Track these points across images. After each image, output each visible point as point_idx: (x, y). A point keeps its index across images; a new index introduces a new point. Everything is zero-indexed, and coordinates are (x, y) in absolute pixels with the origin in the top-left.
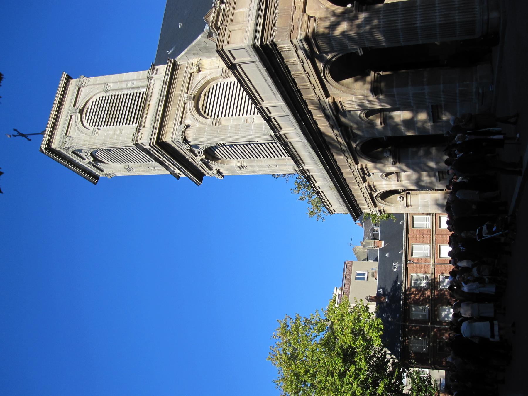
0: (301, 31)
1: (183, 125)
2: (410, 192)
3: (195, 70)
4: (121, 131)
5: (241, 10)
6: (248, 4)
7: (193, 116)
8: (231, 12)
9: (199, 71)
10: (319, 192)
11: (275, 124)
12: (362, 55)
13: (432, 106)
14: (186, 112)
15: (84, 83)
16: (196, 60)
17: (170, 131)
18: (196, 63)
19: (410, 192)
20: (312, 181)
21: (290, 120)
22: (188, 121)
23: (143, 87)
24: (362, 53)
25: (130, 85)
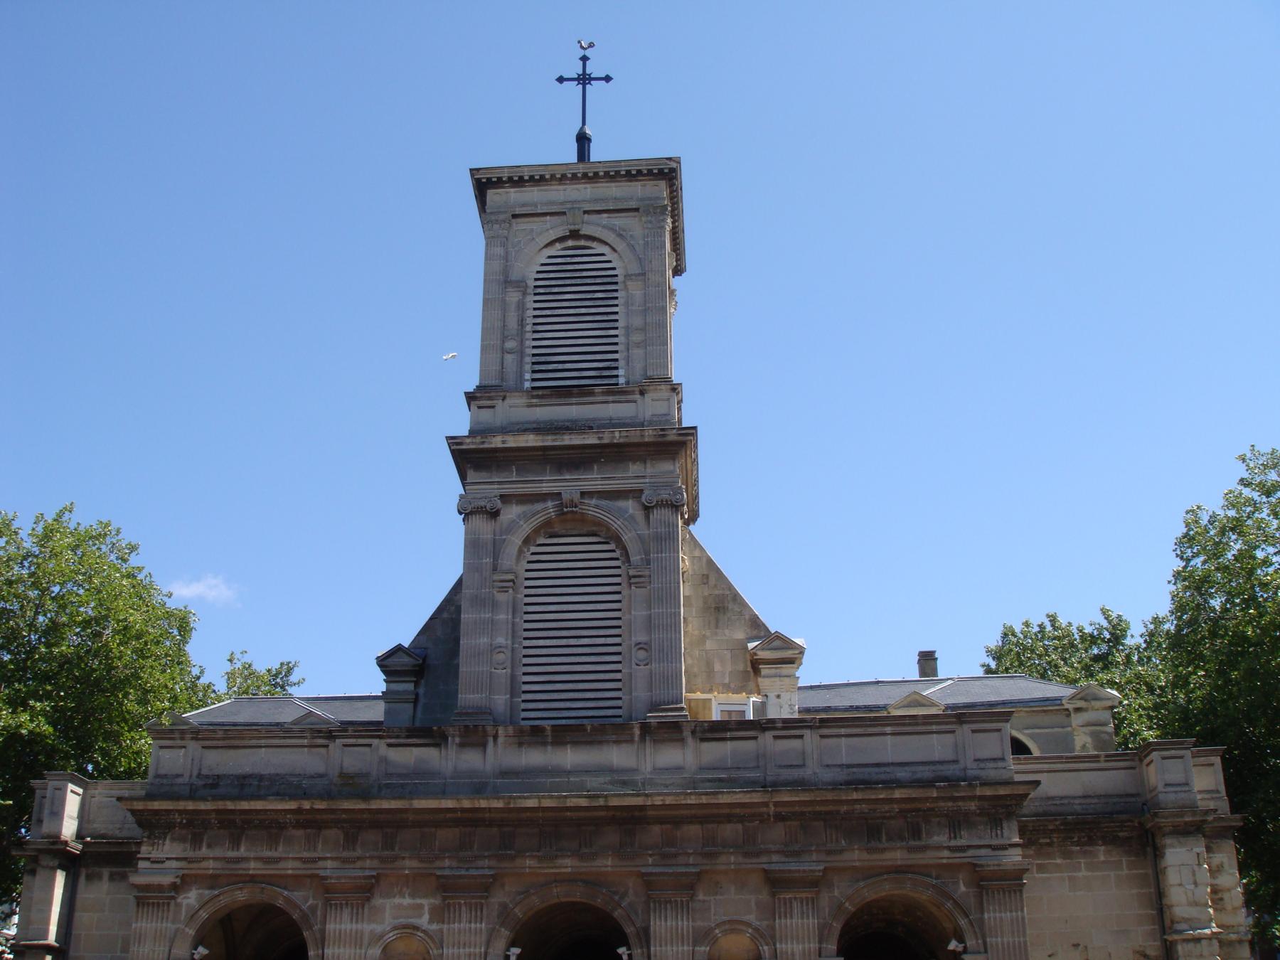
11: (728, 735)
20: (408, 737)
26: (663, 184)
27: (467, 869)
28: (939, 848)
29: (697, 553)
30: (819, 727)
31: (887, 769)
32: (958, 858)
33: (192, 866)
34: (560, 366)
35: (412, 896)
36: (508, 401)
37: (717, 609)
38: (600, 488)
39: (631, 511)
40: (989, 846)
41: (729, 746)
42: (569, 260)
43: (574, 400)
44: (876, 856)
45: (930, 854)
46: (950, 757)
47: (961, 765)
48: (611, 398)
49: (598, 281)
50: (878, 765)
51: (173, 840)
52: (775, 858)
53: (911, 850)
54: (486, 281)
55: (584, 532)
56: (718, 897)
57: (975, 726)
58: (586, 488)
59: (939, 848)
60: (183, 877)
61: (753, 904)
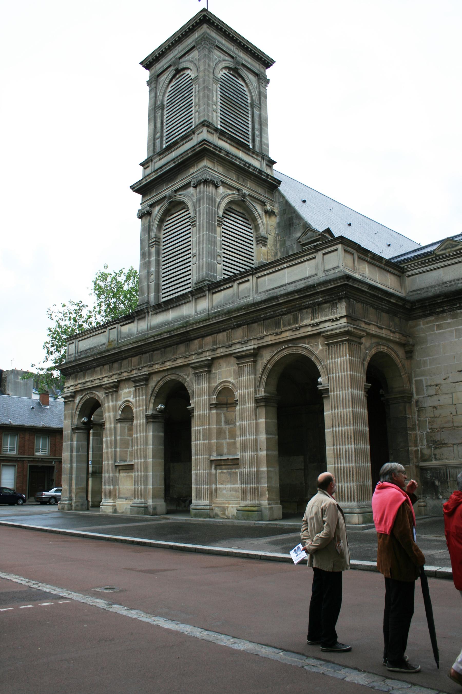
0: (354, 328)
1: (220, 183)
2: (455, 428)
3: (268, 207)
4: (215, 111)
5: (367, 269)
6: (371, 277)
7: (227, 196)
8: (366, 258)
9: (266, 212)
10: (106, 328)
11: (222, 288)
12: (318, 388)
13: (133, 465)
14: (229, 189)
15: (263, 82)
16: (276, 211)
17: (214, 166)
18: (274, 211)
19: (455, 428)
20: (125, 321)
21: (229, 304)
22: (221, 189)
23: (254, 146)
24: (319, 389)
25: (257, 133)
26: (205, 26)
27: (140, 373)
28: (306, 326)
29: (281, 200)
30: (256, 273)
31: (284, 288)
32: (316, 330)
33: (76, 387)
34: (174, 136)
35: (129, 388)
36: (154, 161)
37: (290, 225)
38: (180, 186)
39: (192, 192)
40: (329, 320)
41: (223, 293)
42: (177, 84)
43: (173, 149)
44: (278, 337)
45: (302, 330)
46: (313, 273)
47: (318, 277)
48: (184, 142)
49: (187, 88)
50: (281, 286)
51: (72, 378)
52: (238, 346)
53: (294, 330)
54: (149, 111)
55: (180, 209)
56: (220, 370)
57: (324, 251)
58: (174, 189)
59: (306, 326)
60: (75, 392)
61: (232, 371)
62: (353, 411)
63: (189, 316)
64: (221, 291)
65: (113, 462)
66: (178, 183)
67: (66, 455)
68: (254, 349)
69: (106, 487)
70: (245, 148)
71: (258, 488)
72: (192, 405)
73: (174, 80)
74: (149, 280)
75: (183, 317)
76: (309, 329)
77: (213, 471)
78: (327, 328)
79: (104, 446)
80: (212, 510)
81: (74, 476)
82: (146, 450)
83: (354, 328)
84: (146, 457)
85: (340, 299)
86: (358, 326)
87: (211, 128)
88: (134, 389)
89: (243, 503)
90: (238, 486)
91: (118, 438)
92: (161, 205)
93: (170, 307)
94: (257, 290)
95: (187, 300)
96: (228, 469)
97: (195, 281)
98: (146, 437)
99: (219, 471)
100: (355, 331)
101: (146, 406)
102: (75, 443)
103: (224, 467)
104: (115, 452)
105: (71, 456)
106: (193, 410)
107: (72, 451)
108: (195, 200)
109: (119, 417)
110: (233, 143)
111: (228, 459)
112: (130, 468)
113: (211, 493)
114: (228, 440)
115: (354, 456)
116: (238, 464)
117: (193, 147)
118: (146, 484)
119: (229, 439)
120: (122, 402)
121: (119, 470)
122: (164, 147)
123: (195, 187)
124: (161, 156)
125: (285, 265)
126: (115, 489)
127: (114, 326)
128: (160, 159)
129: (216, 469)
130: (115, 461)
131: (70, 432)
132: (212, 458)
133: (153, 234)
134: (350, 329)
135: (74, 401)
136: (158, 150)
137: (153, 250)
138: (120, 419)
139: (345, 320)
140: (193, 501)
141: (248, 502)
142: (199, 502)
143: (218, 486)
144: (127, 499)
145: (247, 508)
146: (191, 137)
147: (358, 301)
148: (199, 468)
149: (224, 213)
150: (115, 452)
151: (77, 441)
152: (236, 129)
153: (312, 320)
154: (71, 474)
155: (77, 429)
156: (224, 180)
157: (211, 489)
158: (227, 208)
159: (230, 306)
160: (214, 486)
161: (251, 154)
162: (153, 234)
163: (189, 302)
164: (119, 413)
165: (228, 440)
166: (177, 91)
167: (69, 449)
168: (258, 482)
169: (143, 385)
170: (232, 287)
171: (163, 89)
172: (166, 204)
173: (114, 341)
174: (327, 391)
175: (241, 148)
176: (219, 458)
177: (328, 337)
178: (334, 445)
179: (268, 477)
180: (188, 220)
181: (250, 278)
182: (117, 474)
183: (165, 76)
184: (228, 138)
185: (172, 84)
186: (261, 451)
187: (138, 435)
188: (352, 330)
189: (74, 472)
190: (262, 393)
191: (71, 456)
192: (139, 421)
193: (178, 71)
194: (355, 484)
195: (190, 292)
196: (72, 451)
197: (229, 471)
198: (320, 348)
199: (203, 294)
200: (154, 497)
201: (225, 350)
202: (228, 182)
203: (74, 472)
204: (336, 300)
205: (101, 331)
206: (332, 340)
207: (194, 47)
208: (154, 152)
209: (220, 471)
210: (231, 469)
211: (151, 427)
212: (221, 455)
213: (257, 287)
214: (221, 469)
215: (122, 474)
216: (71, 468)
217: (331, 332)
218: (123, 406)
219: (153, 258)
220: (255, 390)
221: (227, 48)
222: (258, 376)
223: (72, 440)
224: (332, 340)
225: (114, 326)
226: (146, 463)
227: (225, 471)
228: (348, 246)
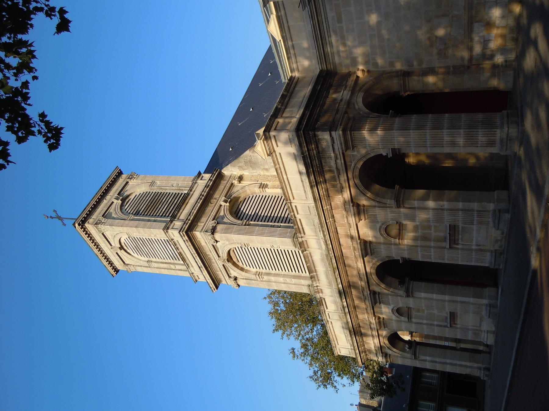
11: (300, 227)
36: (193, 272)
62: (413, 130)
63: (322, 254)
64: (303, 228)
65: (447, 329)
66: (212, 254)
67: (438, 367)
68: (353, 206)
69: (470, 336)
70: (187, 197)
71: (478, 211)
72: (399, 258)
73: (128, 251)
74: (289, 284)
75: (322, 260)
76: (339, 161)
77: (460, 246)
78: (340, 147)
79: (432, 334)
80: (496, 250)
81: (458, 362)
82: (437, 300)
83: (340, 125)
84: (444, 301)
85: (315, 136)
86: (339, 122)
87: (170, 225)
88: (382, 304)
89: (491, 224)
90: (475, 227)
91: (425, 322)
92: (229, 268)
93: (313, 269)
94: (304, 200)
95: (309, 255)
96: (458, 234)
97: (294, 248)
98: (425, 298)
99: (460, 242)
100: (343, 124)
101: (398, 296)
102: (428, 358)
103: (456, 237)
104: (437, 325)
105: (440, 363)
106: (403, 258)
107: (436, 362)
108: (227, 243)
109: (407, 319)
110: (183, 208)
111: (449, 233)
112: (453, 316)
113: (481, 250)
114: (432, 231)
115: (454, 131)
116: (455, 226)
117: (184, 241)
118: (469, 303)
119: (431, 230)
120: (393, 315)
121: (455, 324)
122: (182, 262)
123: (217, 242)
124: (190, 265)
125: (285, 177)
126: (472, 330)
127: (327, 315)
128: (193, 267)
129: (458, 244)
130: (446, 326)
131: (417, 361)
132: (448, 246)
133: (253, 277)
134: (341, 129)
135: (390, 355)
136: (184, 267)
137: (266, 278)
138: (408, 318)
139: (333, 133)
140: (487, 265)
141: (490, 220)
142: (486, 261)
143: (474, 243)
144: (481, 320)
145: (497, 221)
146: (177, 242)
147: (317, 120)
148: (457, 257)
149: (239, 219)
150: (437, 325)
151: (426, 356)
152: (171, 203)
153: (331, 159)
154: (456, 365)
155: (415, 354)
156: (213, 217)
157: (476, 250)
158: (235, 216)
159: (317, 221)
160: (474, 247)
161: (192, 193)
162: (253, 277)
163: (310, 253)
164: (403, 318)
165: (432, 231)
166: (138, 249)
167: (434, 364)
168: (473, 210)
169: (379, 297)
170: (300, 219)
171: (135, 260)
172: (229, 265)
173: (339, 316)
174: (393, 150)
175: (187, 201)
176: (448, 241)
177: (347, 148)
178: (443, 147)
179: (469, 201)
180: (243, 249)
181: (293, 205)
182: (458, 326)
183: (125, 258)
184: (178, 212)
185: (132, 254)
186: (444, 205)
187: (423, 305)
188: (342, 127)
189: (454, 362)
190: (392, 202)
191: (440, 363)
192: (411, 302)
193: (121, 248)
194: (480, 130)
195: (302, 252)
196: (436, 362)
197: (460, 233)
198: (355, 153)
199: (305, 242)
200: (480, 297)
201: (352, 228)
202: (214, 214)
203: (454, 362)
204: (316, 139)
205: (331, 326)
206: (349, 144)
207: (103, 234)
208: (186, 271)
209: (460, 241)
210: (459, 231)
211: (417, 294)
212: (446, 238)
213: (302, 200)
214: (458, 240)
215: (458, 321)
216: (451, 364)
217: (343, 145)
218: (397, 314)
219: (273, 278)
220: (389, 207)
221: (104, 207)
222: (377, 204)
223: (425, 360)
224: (349, 144)
225: (327, 315)
226: (449, 301)
227: (460, 236)
228: (272, 127)
